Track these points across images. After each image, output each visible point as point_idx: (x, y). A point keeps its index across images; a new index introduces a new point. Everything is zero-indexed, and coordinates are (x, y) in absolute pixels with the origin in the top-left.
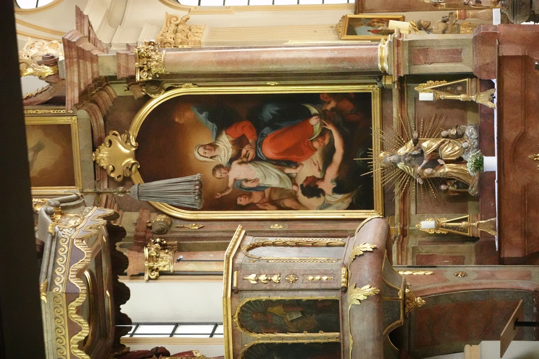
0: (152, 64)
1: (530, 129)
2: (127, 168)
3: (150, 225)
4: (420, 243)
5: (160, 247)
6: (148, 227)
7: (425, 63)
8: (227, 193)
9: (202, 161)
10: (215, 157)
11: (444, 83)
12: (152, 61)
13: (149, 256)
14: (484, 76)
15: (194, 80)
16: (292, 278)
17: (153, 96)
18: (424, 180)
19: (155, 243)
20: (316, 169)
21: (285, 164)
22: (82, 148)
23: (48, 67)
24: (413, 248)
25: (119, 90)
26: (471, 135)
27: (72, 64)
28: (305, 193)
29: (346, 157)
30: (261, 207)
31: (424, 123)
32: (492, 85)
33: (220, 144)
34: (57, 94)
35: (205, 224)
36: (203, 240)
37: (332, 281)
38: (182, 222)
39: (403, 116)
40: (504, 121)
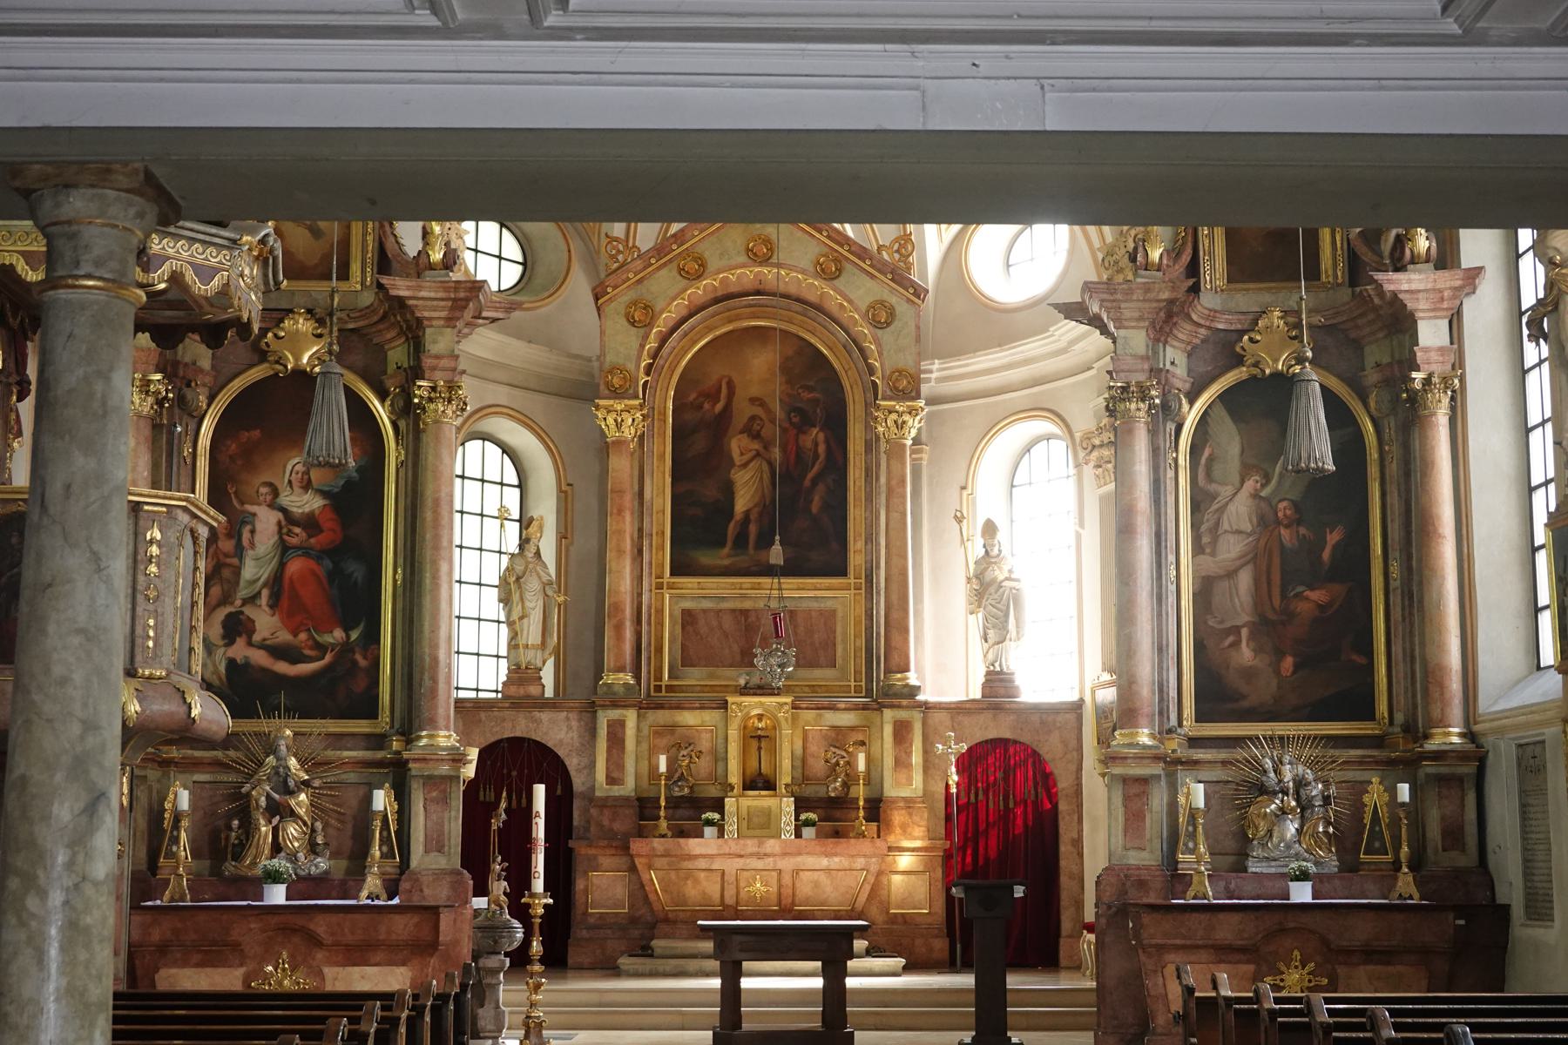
0: (440, 405)
1: (327, 954)
2: (280, 358)
3: (193, 384)
4: (150, 788)
5: (160, 397)
6: (191, 381)
7: (426, 799)
8: (235, 502)
9: (285, 467)
10: (291, 487)
12: (444, 405)
13: (149, 380)
14: (404, 885)
15: (410, 464)
16: (153, 595)
17: (388, 402)
18: (248, 794)
19: (167, 391)
20: (266, 634)
21: (275, 590)
22: (313, 293)
23: (441, 256)
24: (146, 777)
25: (397, 355)
26: (316, 866)
27: (446, 290)
28: (229, 616)
29: (282, 679)
30: (211, 550)
31: (331, 795)
32: (391, 898)
33: (308, 496)
34: (395, 265)
35: (190, 467)
36: (166, 461)
37: (146, 654)
38: (193, 433)
39: (344, 766)
40: (341, 915)
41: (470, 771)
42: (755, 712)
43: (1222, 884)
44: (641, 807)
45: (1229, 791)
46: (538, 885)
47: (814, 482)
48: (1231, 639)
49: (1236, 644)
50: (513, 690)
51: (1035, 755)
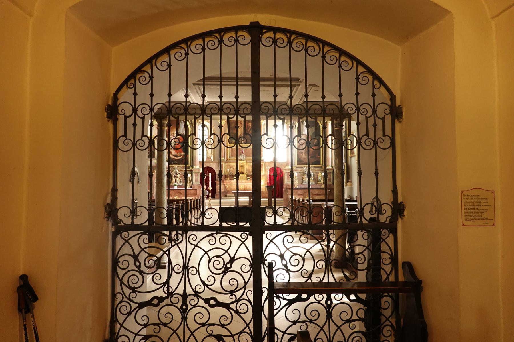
11: (191, 179)
14: (192, 186)
41: (201, 172)
42: (241, 163)
43: (299, 186)
44: (225, 176)
45: (301, 174)
46: (210, 186)
47: (250, 130)
48: (302, 154)
49: (303, 154)
50: (207, 160)
51: (280, 169)
